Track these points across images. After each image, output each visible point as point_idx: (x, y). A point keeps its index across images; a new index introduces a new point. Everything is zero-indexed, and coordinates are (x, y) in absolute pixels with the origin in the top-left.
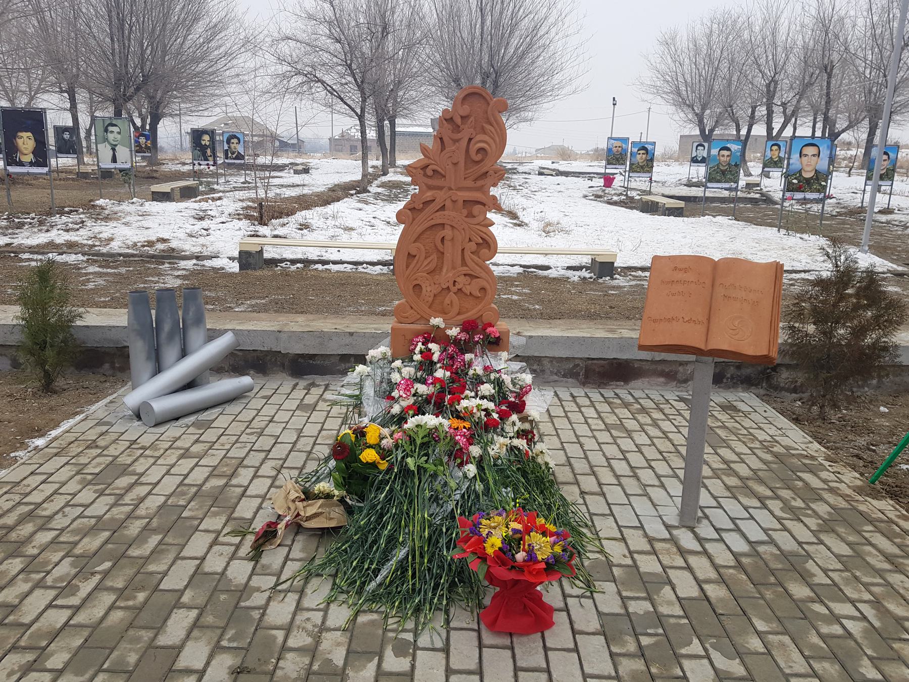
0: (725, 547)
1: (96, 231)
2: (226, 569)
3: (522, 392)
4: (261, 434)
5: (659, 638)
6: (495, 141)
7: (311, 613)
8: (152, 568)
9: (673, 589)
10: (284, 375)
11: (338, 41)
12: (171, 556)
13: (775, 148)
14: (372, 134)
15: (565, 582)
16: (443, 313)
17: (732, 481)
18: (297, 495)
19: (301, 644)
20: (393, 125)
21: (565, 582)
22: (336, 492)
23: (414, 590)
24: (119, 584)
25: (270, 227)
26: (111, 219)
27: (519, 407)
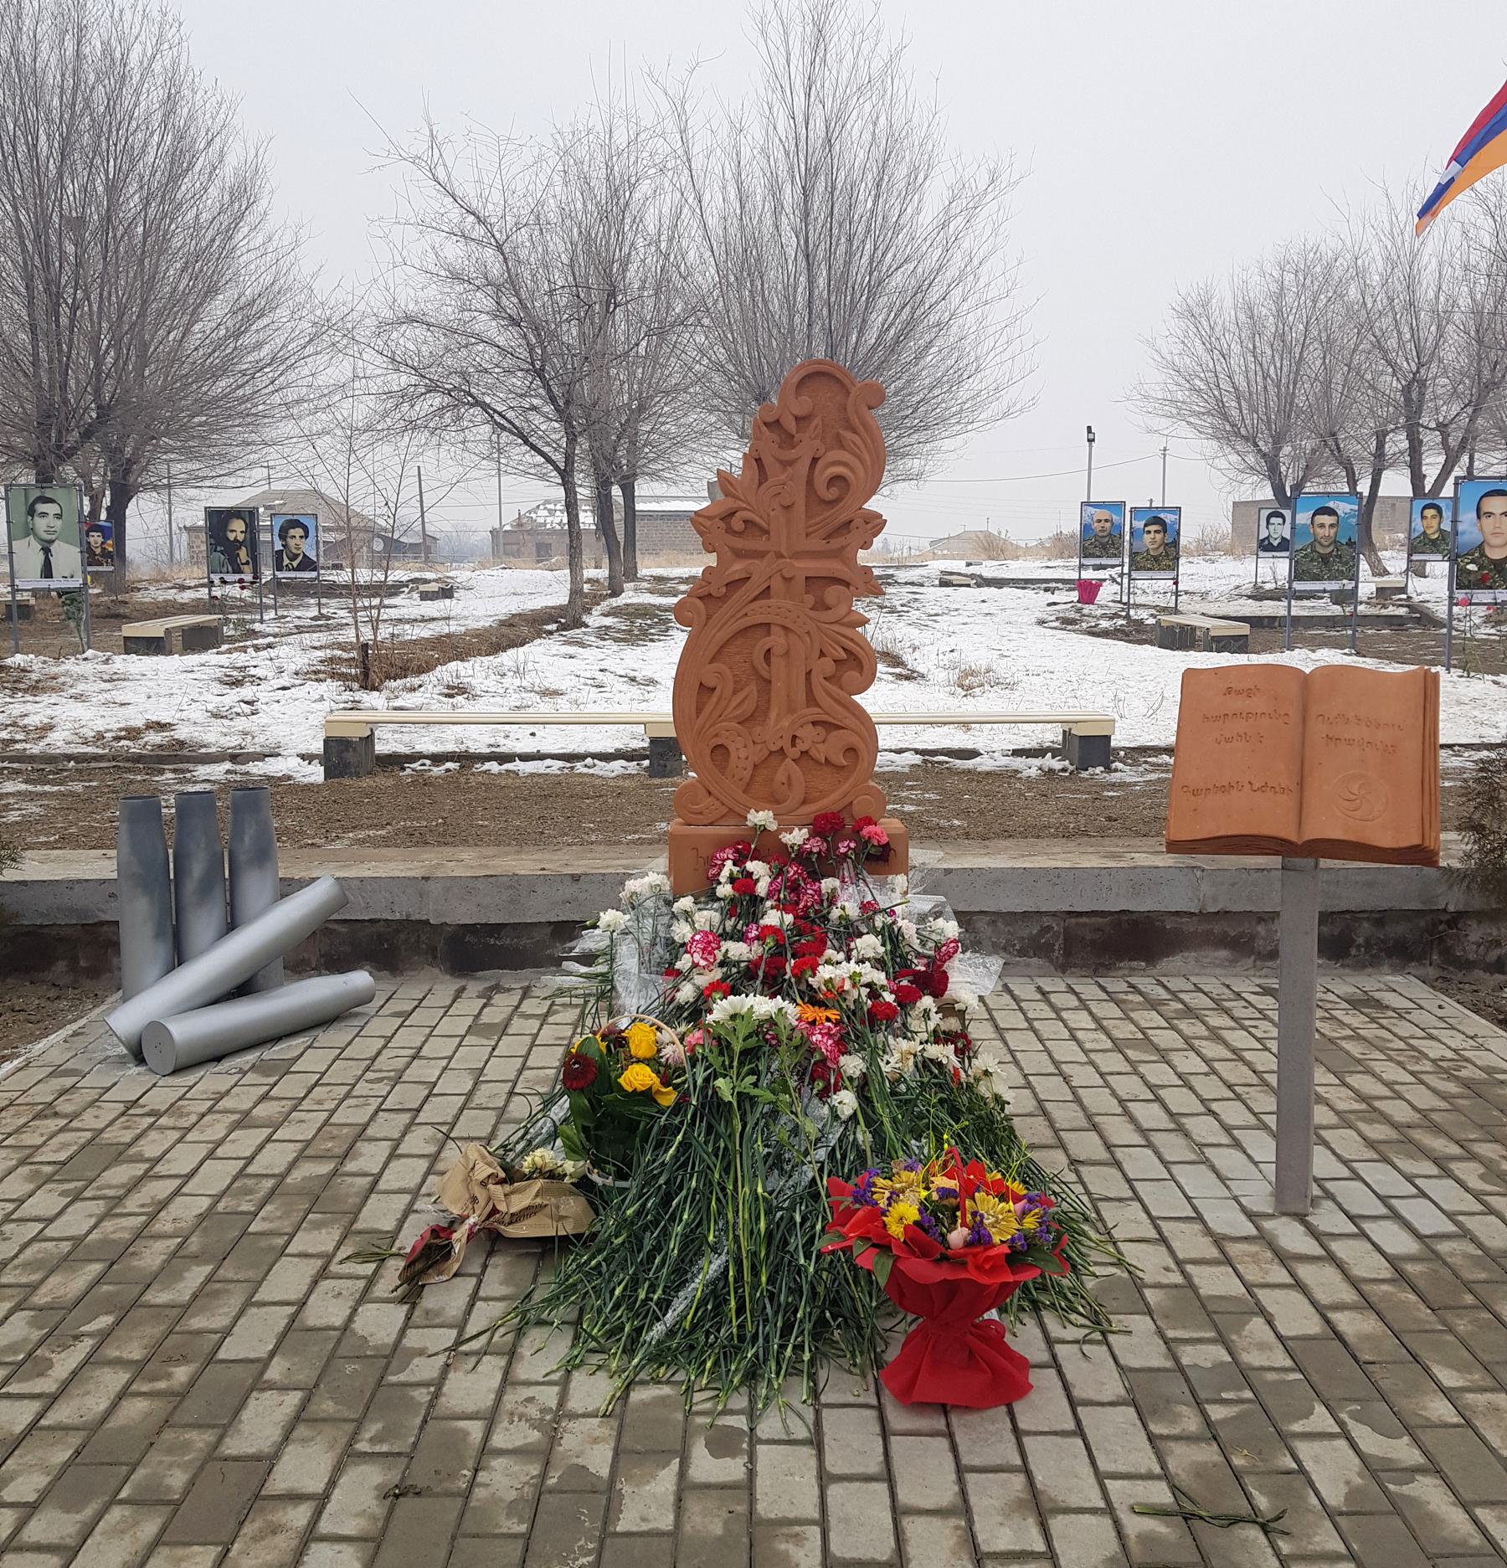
0: (1370, 1247)
1: (16, 713)
2: (350, 1319)
3: (941, 956)
4: (397, 1080)
5: (1245, 1406)
6: (862, 461)
7: (533, 1395)
8: (197, 1323)
9: (1270, 1323)
10: (436, 971)
11: (514, 322)
12: (235, 1302)
13: (1430, 512)
14: (587, 519)
15: (1049, 1319)
16: (772, 800)
17: (1379, 1132)
18: (491, 1171)
19: (519, 1443)
20: (629, 496)
21: (1049, 1319)
22: (569, 1166)
23: (741, 1338)
24: (136, 1353)
25: (385, 693)
26: (44, 690)
27: (934, 981)
